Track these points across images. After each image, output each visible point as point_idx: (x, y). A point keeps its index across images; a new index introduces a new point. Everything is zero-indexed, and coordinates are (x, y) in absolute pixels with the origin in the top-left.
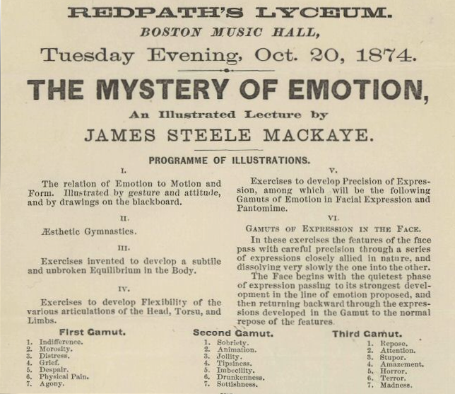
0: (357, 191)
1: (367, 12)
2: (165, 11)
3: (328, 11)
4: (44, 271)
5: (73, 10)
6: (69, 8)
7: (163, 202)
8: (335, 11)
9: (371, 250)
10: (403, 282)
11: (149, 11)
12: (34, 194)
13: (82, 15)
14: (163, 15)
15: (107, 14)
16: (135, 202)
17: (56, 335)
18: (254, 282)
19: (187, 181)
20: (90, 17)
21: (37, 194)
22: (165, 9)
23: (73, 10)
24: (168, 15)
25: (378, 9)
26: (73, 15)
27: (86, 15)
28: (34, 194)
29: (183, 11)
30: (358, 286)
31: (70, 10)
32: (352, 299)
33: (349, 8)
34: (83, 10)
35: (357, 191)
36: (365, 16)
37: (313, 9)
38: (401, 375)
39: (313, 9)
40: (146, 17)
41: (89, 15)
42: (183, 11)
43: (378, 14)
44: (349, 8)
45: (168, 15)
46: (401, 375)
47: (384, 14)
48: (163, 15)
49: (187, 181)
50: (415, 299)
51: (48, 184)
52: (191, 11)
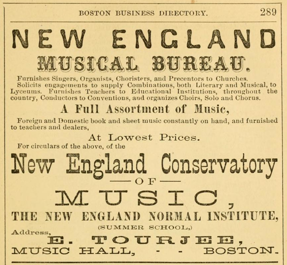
0: (179, 86)
3: (202, 239)
6: (135, 237)
7: (96, 122)
8: (229, 239)
9: (233, 92)
10: (224, 87)
12: (22, 146)
16: (22, 128)
19: (83, 119)
21: (24, 147)
28: (22, 146)
29: (96, 239)
32: (27, 82)
33: (142, 237)
35: (179, 86)
37: (211, 192)
38: (168, 89)
39: (211, 192)
42: (96, 239)
44: (142, 237)
46: (168, 89)
49: (83, 119)
50: (154, 82)
52: (102, 239)
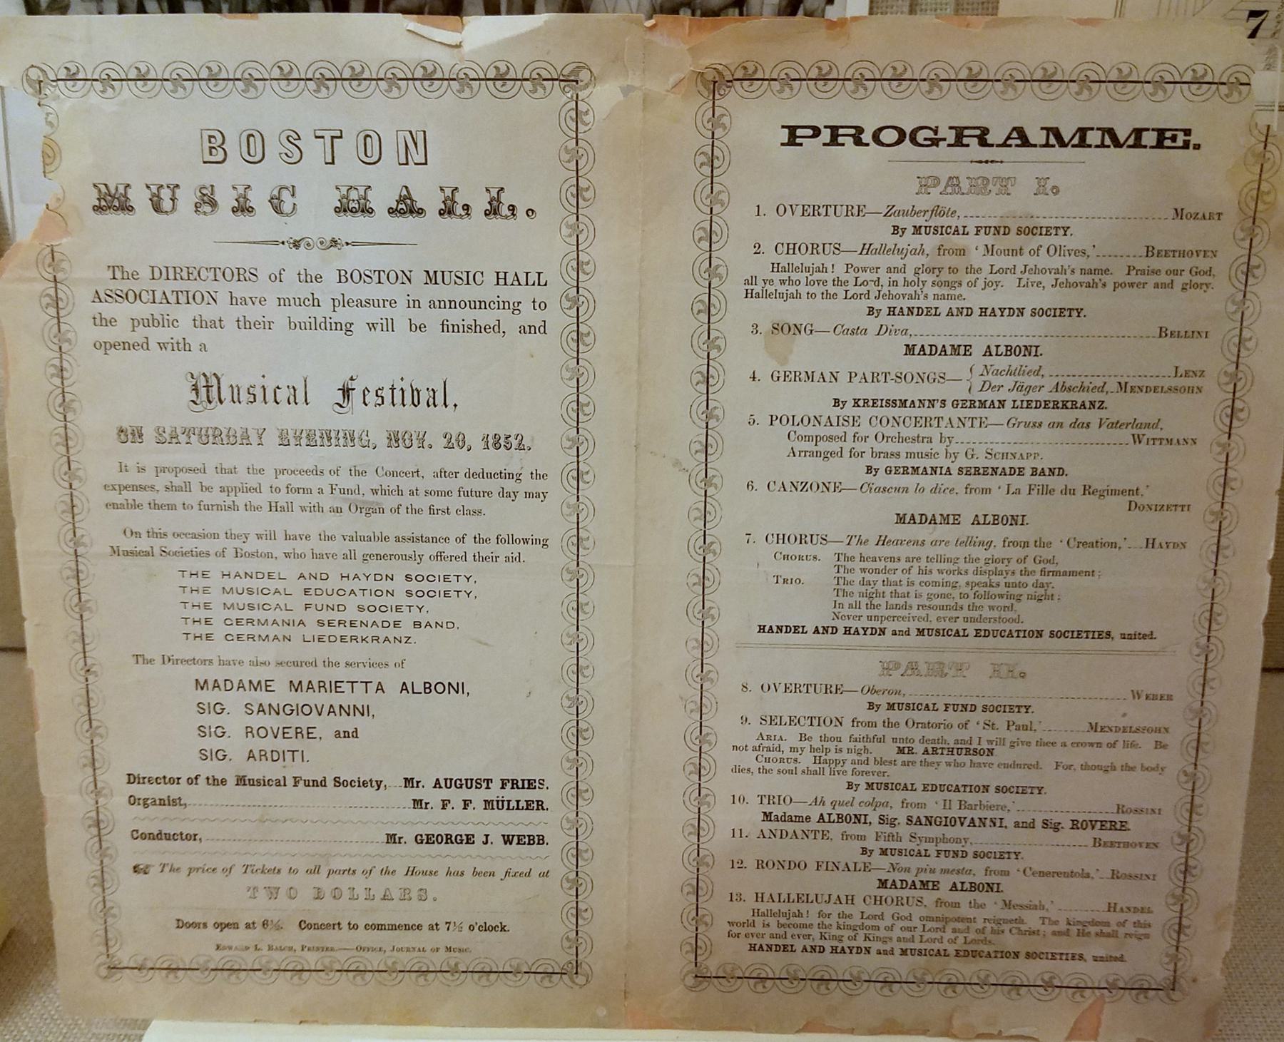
1: (1107, 136)
2: (1015, 135)
4: (153, 345)
5: (792, 130)
11: (810, 132)
13: (851, 139)
14: (1009, 142)
15: (1180, 143)
17: (176, 408)
18: (114, 285)
20: (1035, 146)
22: (1014, 129)
23: (792, 130)
24: (1019, 142)
25: (1080, 129)
26: (792, 141)
27: (858, 142)
30: (846, 606)
31: (954, 131)
33: (1147, 130)
34: (853, 131)
36: (1103, 145)
40: (801, 145)
41: (989, 142)
43: (1076, 141)
45: (1019, 142)
47: (1088, 142)
48: (1009, 142)
51: (842, 558)
